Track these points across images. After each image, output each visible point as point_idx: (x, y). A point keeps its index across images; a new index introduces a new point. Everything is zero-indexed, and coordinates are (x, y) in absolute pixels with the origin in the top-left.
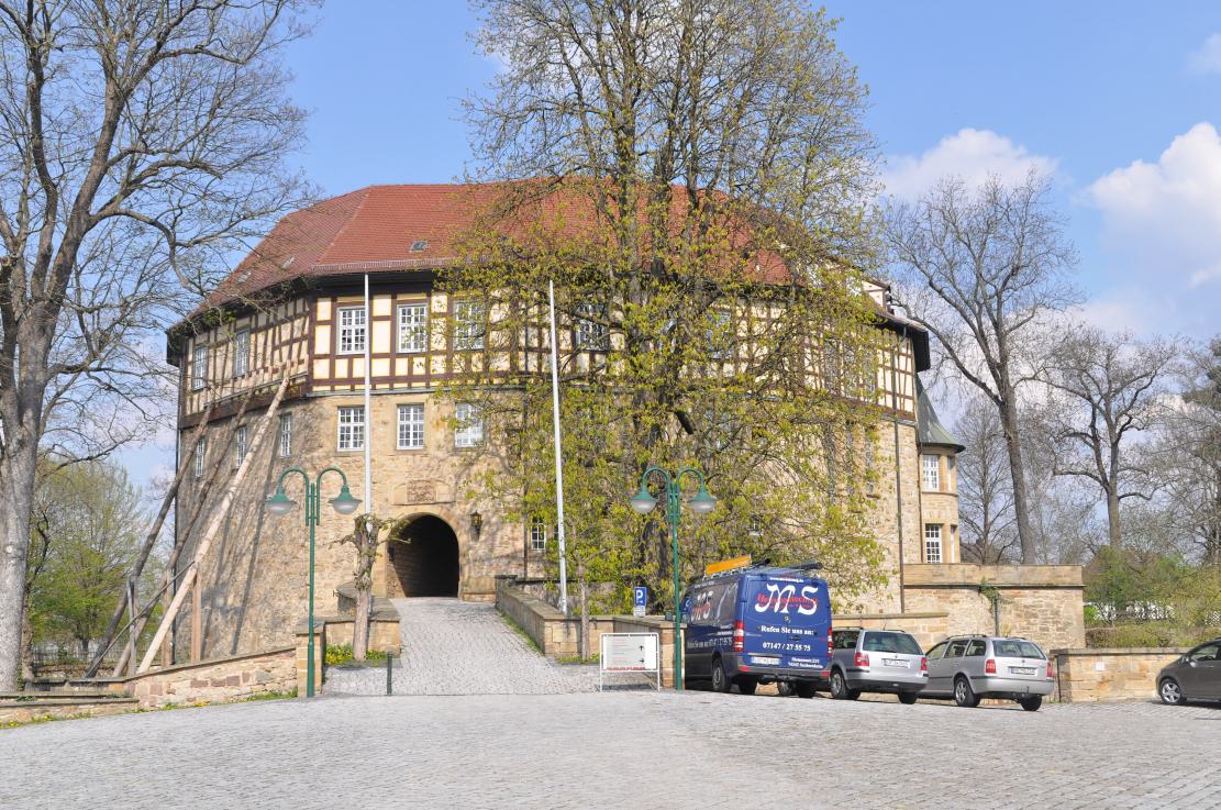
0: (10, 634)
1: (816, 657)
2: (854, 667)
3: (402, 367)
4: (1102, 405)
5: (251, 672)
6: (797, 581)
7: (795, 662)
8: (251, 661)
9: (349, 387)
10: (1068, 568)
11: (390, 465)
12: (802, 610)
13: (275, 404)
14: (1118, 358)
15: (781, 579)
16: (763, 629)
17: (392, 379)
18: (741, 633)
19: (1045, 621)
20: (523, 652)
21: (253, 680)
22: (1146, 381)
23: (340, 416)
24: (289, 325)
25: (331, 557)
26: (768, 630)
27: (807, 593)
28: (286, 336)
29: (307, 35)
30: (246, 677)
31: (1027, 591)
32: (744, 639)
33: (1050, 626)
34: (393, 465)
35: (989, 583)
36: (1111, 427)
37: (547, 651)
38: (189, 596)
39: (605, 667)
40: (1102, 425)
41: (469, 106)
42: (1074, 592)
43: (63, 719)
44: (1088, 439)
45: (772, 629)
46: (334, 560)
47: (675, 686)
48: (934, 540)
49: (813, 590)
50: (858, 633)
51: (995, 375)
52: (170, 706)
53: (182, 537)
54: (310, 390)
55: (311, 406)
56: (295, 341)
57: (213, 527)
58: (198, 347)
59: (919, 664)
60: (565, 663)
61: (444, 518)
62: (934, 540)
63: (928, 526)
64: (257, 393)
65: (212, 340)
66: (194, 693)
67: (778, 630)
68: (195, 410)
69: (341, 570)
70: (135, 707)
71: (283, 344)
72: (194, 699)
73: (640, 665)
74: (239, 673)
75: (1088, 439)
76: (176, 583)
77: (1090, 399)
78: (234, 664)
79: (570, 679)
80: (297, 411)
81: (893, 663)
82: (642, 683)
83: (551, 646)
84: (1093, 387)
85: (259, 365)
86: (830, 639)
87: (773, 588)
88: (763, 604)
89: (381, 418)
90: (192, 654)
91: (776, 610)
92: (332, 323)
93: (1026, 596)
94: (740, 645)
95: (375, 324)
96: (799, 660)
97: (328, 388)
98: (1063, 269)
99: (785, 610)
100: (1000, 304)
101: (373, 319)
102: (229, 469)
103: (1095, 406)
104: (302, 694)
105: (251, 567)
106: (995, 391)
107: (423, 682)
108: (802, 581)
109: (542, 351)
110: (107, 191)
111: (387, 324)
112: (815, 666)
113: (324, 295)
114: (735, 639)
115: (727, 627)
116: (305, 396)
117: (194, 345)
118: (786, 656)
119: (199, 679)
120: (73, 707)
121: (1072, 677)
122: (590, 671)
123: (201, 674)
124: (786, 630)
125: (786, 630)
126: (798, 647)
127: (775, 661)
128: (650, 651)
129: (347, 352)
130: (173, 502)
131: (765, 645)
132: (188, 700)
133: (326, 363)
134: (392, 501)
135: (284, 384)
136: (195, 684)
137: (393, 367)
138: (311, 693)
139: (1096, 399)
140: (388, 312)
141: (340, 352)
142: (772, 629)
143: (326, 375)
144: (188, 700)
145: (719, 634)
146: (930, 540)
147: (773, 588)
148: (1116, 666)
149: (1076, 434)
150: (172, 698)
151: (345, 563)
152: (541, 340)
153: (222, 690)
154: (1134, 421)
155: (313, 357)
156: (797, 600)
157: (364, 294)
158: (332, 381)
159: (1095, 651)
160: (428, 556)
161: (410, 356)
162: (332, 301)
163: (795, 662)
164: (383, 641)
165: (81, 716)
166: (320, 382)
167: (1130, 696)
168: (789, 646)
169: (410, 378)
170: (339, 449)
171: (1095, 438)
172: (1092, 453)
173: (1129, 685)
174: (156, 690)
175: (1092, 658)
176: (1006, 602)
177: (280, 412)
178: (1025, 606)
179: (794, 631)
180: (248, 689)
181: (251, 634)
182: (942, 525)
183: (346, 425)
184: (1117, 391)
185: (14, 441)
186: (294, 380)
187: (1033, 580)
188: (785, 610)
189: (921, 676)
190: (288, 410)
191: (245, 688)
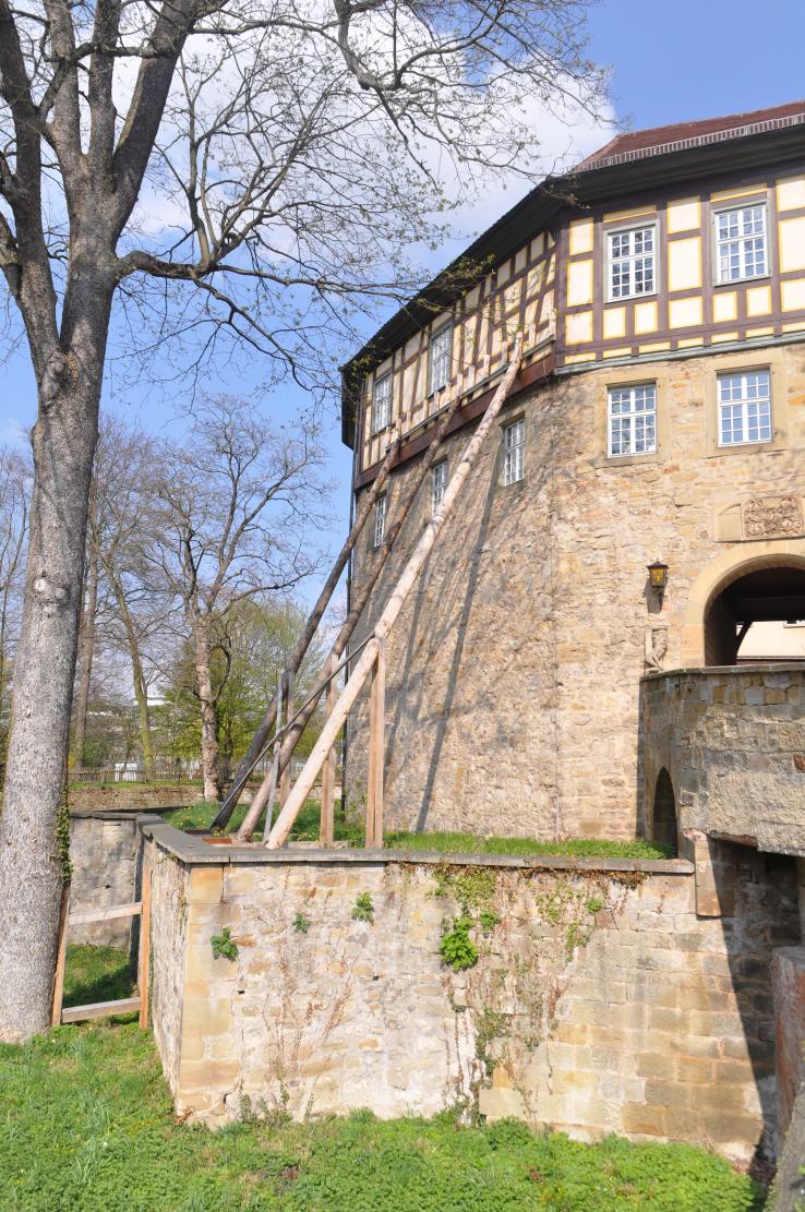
0: (42, 748)
3: (725, 307)
9: (628, 351)
11: (707, 473)
13: (495, 404)
17: (708, 328)
23: (610, 402)
25: (602, 635)
34: (715, 474)
38: (364, 694)
46: (607, 640)
53: (356, 606)
55: (562, 390)
57: (407, 581)
64: (465, 402)
69: (618, 659)
76: (349, 666)
80: (536, 407)
85: (468, 358)
89: (687, 397)
90: (369, 796)
92: (595, 255)
95: (675, 248)
97: (592, 356)
102: (421, 522)
105: (457, 661)
113: (577, 214)
116: (551, 375)
117: (375, 379)
130: (344, 575)
133: (587, 317)
134: (715, 534)
135: (512, 369)
137: (663, 315)
140: (695, 224)
143: (587, 337)
151: (627, 645)
155: (563, 312)
158: (599, 344)
161: (740, 287)
162: (595, 222)
166: (580, 348)
170: (610, 454)
177: (503, 418)
181: (455, 764)
186: (530, 357)
190: (516, 412)
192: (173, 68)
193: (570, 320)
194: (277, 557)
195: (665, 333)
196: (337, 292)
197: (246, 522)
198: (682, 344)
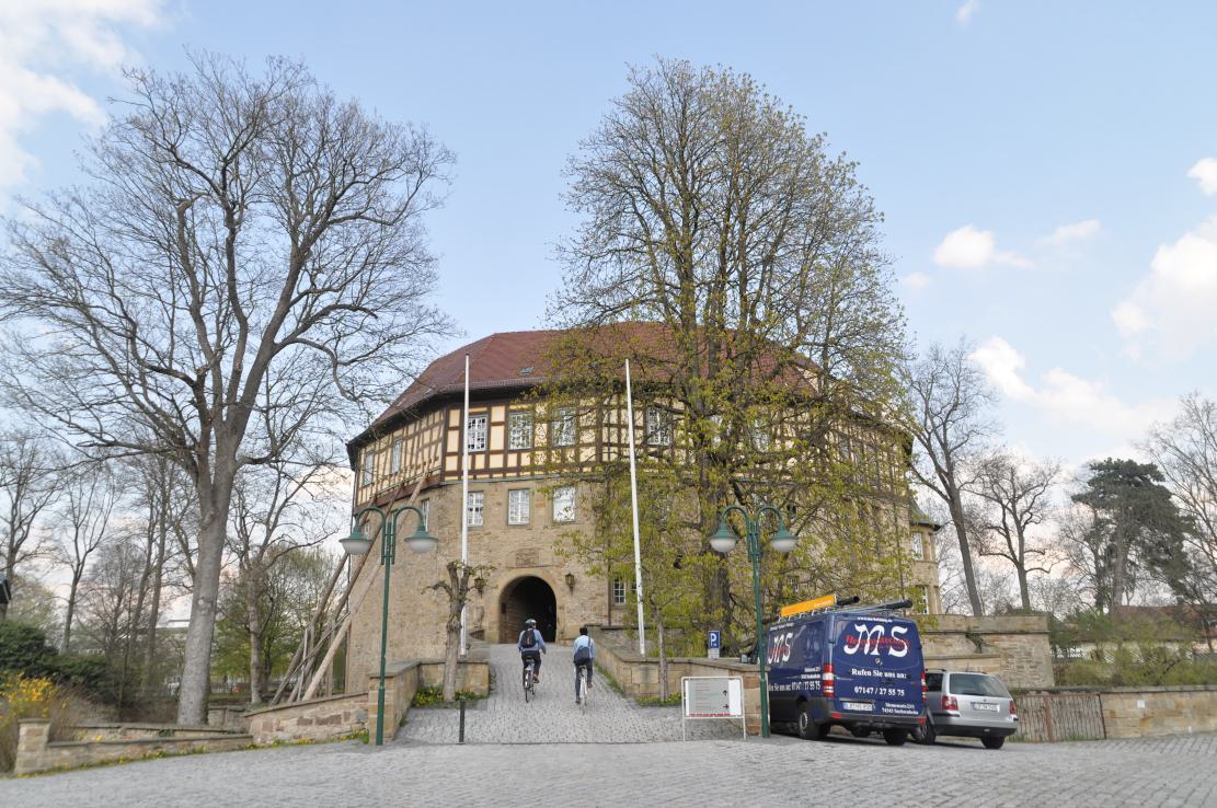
0: (199, 672)
1: (910, 702)
2: (941, 711)
3: (512, 461)
4: (1010, 506)
5: (352, 711)
6: (886, 621)
7: (889, 708)
8: (352, 701)
12: (892, 652)
14: (1019, 474)
15: (870, 619)
16: (854, 672)
17: (505, 470)
18: (829, 676)
19: (1020, 660)
20: (605, 693)
21: (353, 719)
22: (1040, 489)
24: (429, 432)
26: (859, 673)
27: (897, 634)
28: (427, 441)
29: (440, 206)
30: (347, 716)
31: (1004, 637)
32: (833, 683)
35: (973, 631)
36: (1018, 522)
37: (628, 692)
39: (688, 714)
40: (1010, 521)
41: (561, 249)
43: (174, 755)
44: (1001, 531)
45: (863, 673)
50: (942, 675)
51: (944, 482)
52: (279, 743)
54: (442, 479)
56: (433, 443)
58: (367, 454)
59: (1008, 708)
60: (644, 705)
61: (546, 580)
65: (377, 448)
66: (302, 730)
67: (869, 673)
68: (364, 501)
71: (425, 446)
72: (300, 737)
73: (723, 711)
74: (341, 712)
75: (1001, 531)
77: (1001, 502)
79: (651, 724)
80: (433, 495)
81: (982, 707)
82: (726, 729)
83: (631, 688)
84: (1002, 495)
85: (408, 463)
86: (924, 683)
87: (862, 629)
88: (852, 646)
91: (866, 652)
93: (1003, 640)
94: (830, 690)
95: (494, 429)
96: (894, 706)
98: (989, 405)
99: (875, 652)
100: (945, 430)
101: (491, 424)
103: (1004, 507)
104: (373, 740)
106: (945, 492)
107: (502, 727)
108: (890, 621)
109: (621, 426)
110: (289, 324)
111: (502, 428)
112: (909, 712)
114: (824, 683)
115: (814, 670)
118: (880, 701)
119: (305, 717)
120: (186, 743)
121: (1118, 715)
122: (668, 715)
123: (307, 713)
125: (878, 674)
126: (892, 692)
127: (868, 707)
128: (737, 696)
131: (856, 689)
132: (295, 737)
136: (302, 722)
137: (487, 461)
138: (380, 742)
139: (1005, 502)
142: (863, 673)
144: (295, 737)
145: (803, 677)
147: (862, 629)
148: (1155, 703)
149: (992, 527)
150: (281, 735)
152: (619, 436)
153: (325, 728)
154: (1034, 517)
155: (445, 454)
156: (886, 642)
157: (471, 392)
159: (1136, 690)
160: (531, 603)
161: (519, 452)
163: (889, 708)
164: (472, 683)
165: (194, 752)
167: (1170, 732)
168: (883, 691)
169: (519, 469)
171: (1006, 529)
172: (1005, 540)
173: (1169, 721)
174: (268, 727)
175: (1132, 695)
176: (986, 645)
178: (1004, 649)
179: (886, 675)
180: (348, 728)
182: (927, 586)
184: (1020, 497)
185: (208, 516)
187: (1009, 627)
188: (875, 652)
189: (1012, 720)
191: (346, 727)
192: (259, 382)
193: (448, 459)
194: (308, 524)
195: (487, 470)
196: (361, 289)
197: (286, 500)
198: (495, 476)
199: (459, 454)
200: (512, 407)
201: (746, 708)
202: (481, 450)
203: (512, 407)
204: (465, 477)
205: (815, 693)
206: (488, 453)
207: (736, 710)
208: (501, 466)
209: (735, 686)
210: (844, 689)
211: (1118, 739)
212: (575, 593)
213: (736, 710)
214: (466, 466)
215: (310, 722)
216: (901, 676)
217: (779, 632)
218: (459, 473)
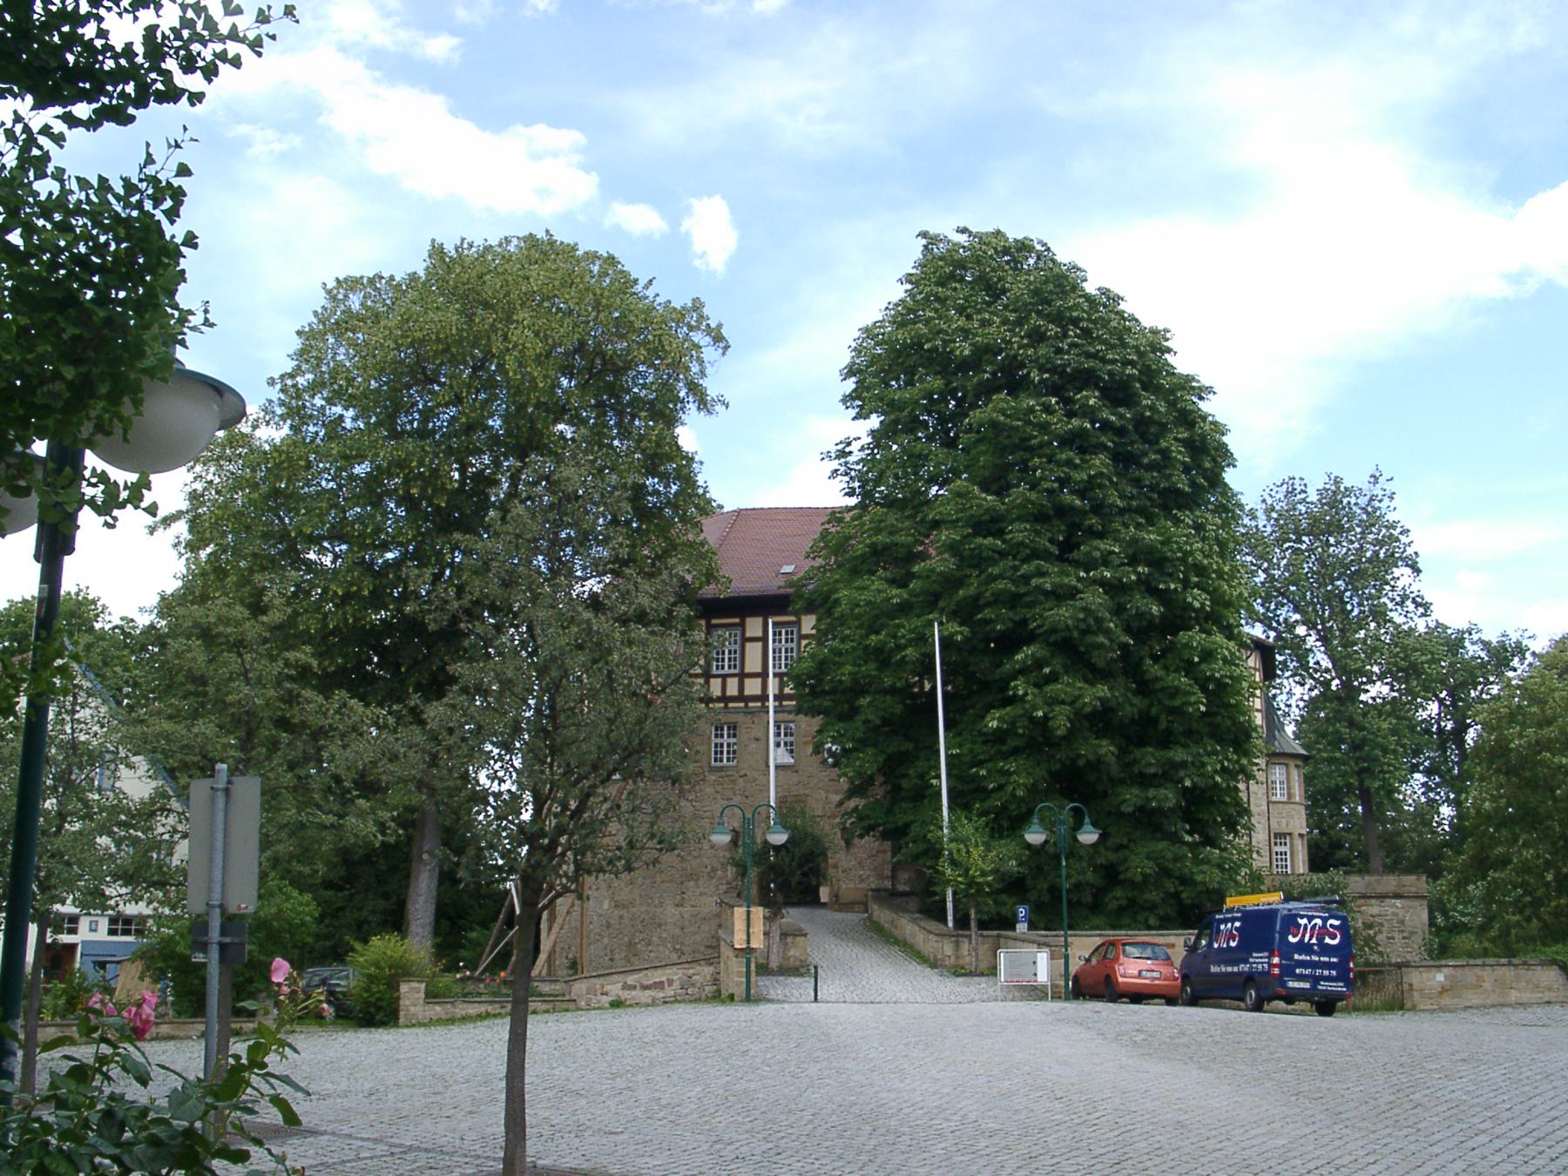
8: (674, 969)
10: (1414, 877)
12: (1327, 940)
16: (1296, 957)
18: (1276, 960)
21: (676, 985)
30: (670, 982)
33: (1396, 935)
42: (1416, 903)
45: (1303, 957)
47: (1067, 999)
48: (1283, 849)
49: (1337, 923)
60: (957, 974)
62: (1283, 849)
63: (1276, 835)
70: (572, 1006)
74: (664, 979)
78: (659, 971)
82: (1036, 993)
87: (1303, 922)
95: (748, 645)
99: (1314, 941)
101: (745, 640)
114: (1271, 965)
118: (1316, 980)
124: (1315, 958)
125: (1315, 958)
126: (1326, 973)
127: (1307, 985)
129: (720, 672)
136: (626, 987)
137: (741, 687)
141: (714, 671)
142: (1303, 957)
146: (1278, 849)
147: (1303, 922)
156: (1323, 932)
163: (1323, 986)
168: (1319, 972)
183: (719, 740)
195: (741, 697)
199: (764, 675)
200: (714, 621)
201: (1052, 977)
202: (733, 671)
203: (714, 621)
204: (771, 704)
205: (1263, 973)
206: (743, 676)
207: (1043, 977)
208: (759, 692)
209: (1043, 958)
210: (1288, 971)
211: (1414, 1008)
212: (852, 851)
213: (1043, 977)
214: (772, 690)
215: (635, 987)
216: (1334, 960)
217: (1225, 921)
218: (763, 698)
